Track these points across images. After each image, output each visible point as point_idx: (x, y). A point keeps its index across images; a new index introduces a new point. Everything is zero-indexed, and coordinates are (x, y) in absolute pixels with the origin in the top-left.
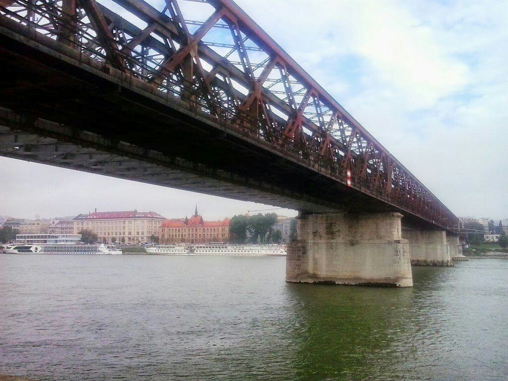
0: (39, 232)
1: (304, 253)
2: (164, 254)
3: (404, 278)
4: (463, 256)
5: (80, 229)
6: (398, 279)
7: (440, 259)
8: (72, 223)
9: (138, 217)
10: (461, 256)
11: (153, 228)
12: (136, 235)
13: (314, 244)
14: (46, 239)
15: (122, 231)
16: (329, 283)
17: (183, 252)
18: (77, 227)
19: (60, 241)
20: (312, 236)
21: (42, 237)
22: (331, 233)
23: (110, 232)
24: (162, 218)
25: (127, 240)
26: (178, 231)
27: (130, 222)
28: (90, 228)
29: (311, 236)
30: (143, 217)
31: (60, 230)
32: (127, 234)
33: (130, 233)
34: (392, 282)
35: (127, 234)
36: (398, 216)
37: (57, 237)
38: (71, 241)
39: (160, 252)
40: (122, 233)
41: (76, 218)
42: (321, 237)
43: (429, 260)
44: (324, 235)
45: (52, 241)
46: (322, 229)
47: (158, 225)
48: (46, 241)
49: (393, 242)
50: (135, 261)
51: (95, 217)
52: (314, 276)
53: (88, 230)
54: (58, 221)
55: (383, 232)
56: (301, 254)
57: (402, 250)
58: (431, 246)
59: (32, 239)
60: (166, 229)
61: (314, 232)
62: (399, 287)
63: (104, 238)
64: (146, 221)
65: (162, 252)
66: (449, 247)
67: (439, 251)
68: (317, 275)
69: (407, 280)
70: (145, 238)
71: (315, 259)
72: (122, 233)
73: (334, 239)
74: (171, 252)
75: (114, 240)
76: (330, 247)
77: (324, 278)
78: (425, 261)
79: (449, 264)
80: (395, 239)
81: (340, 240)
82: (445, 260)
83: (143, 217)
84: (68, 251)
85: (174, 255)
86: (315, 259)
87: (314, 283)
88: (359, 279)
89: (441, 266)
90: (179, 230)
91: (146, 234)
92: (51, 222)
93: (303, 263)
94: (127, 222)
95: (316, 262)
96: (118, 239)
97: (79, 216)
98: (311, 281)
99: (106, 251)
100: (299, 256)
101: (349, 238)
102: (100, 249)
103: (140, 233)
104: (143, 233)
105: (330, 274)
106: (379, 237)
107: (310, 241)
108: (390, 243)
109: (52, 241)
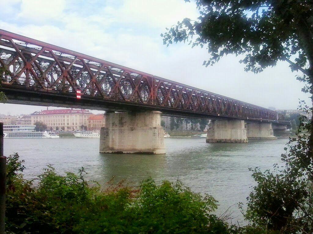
0: (10, 123)
1: (108, 135)
2: (85, 138)
3: (158, 149)
4: (274, 137)
5: (36, 121)
6: (154, 149)
7: (239, 139)
8: (30, 117)
9: (74, 113)
10: (272, 136)
11: (84, 120)
12: (72, 125)
13: (113, 130)
14: (12, 128)
15: (63, 122)
16: (120, 153)
17: (98, 136)
18: (33, 120)
19: (21, 129)
20: (112, 125)
21: (9, 127)
22: (122, 124)
23: (53, 123)
24: (90, 114)
25: (66, 128)
26: (99, 122)
27: (68, 117)
28: (42, 121)
29: (111, 125)
30: (76, 113)
31: (24, 122)
32: (66, 125)
33: (68, 124)
34: (151, 151)
35: (66, 125)
36: (158, 113)
37: (19, 127)
38: (29, 129)
39: (83, 136)
40: (63, 124)
41: (33, 114)
42: (116, 126)
43: (232, 139)
44: (118, 124)
45: (16, 129)
46: (117, 122)
47: (87, 118)
48: (12, 129)
49: (153, 128)
50: (68, 142)
51: (45, 113)
52: (112, 149)
53: (41, 122)
54: (22, 117)
55: (147, 122)
56: (106, 136)
57: (157, 133)
58: (234, 130)
59: (5, 129)
60: (92, 121)
61: (113, 123)
62: (154, 154)
63: (51, 127)
64: (78, 116)
65: (85, 136)
66: (245, 131)
67: (239, 134)
68: (114, 148)
69: (161, 150)
70: (78, 127)
71: (113, 139)
72: (63, 124)
73: (123, 127)
74: (90, 136)
75: (57, 129)
76: (121, 132)
77: (117, 150)
78: (230, 140)
79: (245, 142)
80: (154, 126)
81: (126, 127)
82: (242, 139)
83: (76, 113)
84: (24, 136)
85: (92, 138)
86: (113, 139)
87: (112, 153)
88: (135, 150)
89: (239, 143)
90: (100, 122)
91: (78, 125)
92: (18, 117)
93: (106, 141)
94: (66, 116)
95: (113, 141)
96: (60, 128)
97: (35, 113)
98: (110, 152)
99: (48, 136)
100: (105, 137)
101: (131, 126)
102: (44, 135)
103: (75, 124)
104: (76, 124)
105: (121, 148)
106: (146, 125)
107: (111, 128)
108: (151, 129)
109: (16, 129)
